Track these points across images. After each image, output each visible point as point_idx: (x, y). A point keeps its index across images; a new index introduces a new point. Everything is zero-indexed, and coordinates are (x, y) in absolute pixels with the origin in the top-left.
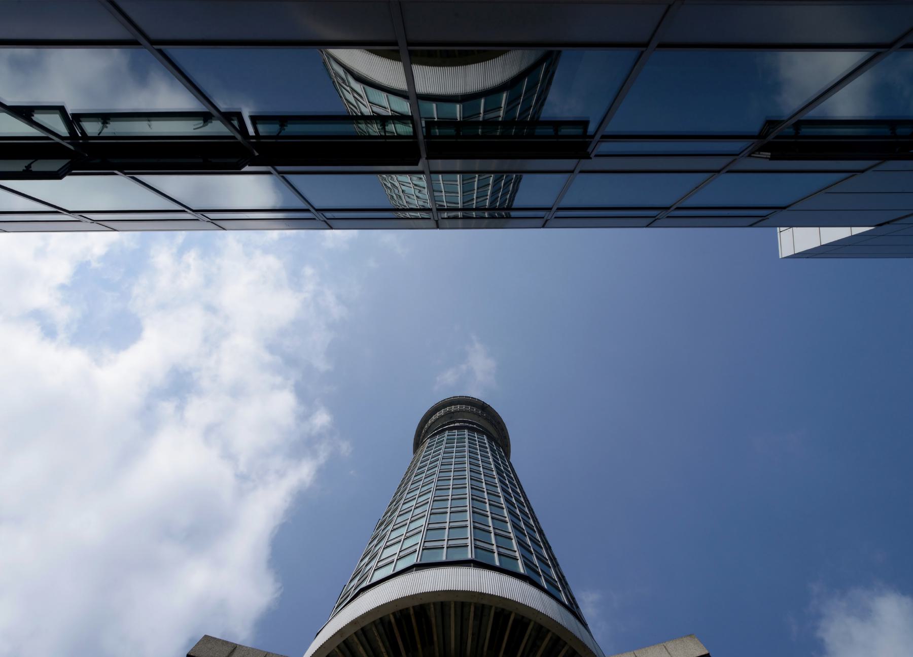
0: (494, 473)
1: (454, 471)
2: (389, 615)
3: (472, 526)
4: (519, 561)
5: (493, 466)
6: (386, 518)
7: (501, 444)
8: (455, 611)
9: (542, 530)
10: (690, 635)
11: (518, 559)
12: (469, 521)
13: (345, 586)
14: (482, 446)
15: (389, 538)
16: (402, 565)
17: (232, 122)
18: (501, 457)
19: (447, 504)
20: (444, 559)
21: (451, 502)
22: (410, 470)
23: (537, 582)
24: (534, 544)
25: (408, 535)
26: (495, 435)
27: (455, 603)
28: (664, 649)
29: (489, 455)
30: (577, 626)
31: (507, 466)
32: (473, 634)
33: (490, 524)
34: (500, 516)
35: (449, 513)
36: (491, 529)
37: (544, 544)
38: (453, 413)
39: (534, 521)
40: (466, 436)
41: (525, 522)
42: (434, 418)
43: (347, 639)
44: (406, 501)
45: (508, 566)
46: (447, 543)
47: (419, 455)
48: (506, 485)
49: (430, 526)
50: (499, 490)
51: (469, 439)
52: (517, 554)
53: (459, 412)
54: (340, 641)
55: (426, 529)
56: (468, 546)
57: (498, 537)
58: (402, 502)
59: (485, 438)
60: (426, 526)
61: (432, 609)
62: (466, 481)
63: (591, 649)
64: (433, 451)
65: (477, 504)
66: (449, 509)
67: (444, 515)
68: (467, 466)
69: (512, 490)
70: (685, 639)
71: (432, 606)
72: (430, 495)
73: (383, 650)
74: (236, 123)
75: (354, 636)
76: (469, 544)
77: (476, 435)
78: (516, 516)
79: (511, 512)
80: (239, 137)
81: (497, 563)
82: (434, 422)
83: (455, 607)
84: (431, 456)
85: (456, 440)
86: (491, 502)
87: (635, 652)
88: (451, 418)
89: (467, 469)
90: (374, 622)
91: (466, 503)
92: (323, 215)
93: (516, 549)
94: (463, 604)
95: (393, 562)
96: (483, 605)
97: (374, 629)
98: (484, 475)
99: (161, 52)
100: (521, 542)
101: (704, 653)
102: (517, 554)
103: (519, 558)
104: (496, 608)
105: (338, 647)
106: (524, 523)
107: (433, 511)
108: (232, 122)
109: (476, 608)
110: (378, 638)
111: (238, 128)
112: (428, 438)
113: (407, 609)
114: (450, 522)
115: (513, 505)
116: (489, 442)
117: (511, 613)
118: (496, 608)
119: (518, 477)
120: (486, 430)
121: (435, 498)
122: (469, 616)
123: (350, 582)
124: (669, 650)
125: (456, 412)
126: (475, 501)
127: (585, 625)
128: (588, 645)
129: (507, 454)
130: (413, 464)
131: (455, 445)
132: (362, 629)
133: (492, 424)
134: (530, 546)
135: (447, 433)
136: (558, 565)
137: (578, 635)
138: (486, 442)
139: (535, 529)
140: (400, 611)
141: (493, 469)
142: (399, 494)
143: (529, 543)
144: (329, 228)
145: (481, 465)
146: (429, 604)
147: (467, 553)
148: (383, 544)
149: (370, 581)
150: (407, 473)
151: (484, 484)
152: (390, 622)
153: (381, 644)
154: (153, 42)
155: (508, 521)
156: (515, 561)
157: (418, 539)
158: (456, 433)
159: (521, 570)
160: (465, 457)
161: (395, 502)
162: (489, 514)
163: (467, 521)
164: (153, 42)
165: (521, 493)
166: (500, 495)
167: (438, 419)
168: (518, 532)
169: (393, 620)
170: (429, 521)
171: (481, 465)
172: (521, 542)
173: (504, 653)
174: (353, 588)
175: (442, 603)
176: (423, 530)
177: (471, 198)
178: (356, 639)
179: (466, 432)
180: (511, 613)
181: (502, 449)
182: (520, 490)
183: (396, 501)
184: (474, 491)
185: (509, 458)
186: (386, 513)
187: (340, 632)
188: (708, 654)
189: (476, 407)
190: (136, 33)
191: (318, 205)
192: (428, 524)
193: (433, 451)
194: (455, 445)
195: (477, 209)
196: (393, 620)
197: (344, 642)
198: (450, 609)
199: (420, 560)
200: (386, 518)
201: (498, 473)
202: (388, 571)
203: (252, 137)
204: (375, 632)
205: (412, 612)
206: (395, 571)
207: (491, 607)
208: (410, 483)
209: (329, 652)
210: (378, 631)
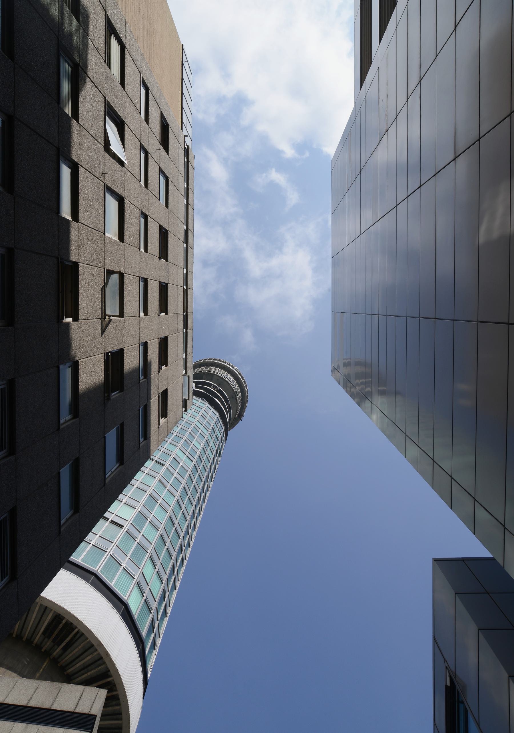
104: (113, 679)
125: (237, 400)
205: (115, 693)
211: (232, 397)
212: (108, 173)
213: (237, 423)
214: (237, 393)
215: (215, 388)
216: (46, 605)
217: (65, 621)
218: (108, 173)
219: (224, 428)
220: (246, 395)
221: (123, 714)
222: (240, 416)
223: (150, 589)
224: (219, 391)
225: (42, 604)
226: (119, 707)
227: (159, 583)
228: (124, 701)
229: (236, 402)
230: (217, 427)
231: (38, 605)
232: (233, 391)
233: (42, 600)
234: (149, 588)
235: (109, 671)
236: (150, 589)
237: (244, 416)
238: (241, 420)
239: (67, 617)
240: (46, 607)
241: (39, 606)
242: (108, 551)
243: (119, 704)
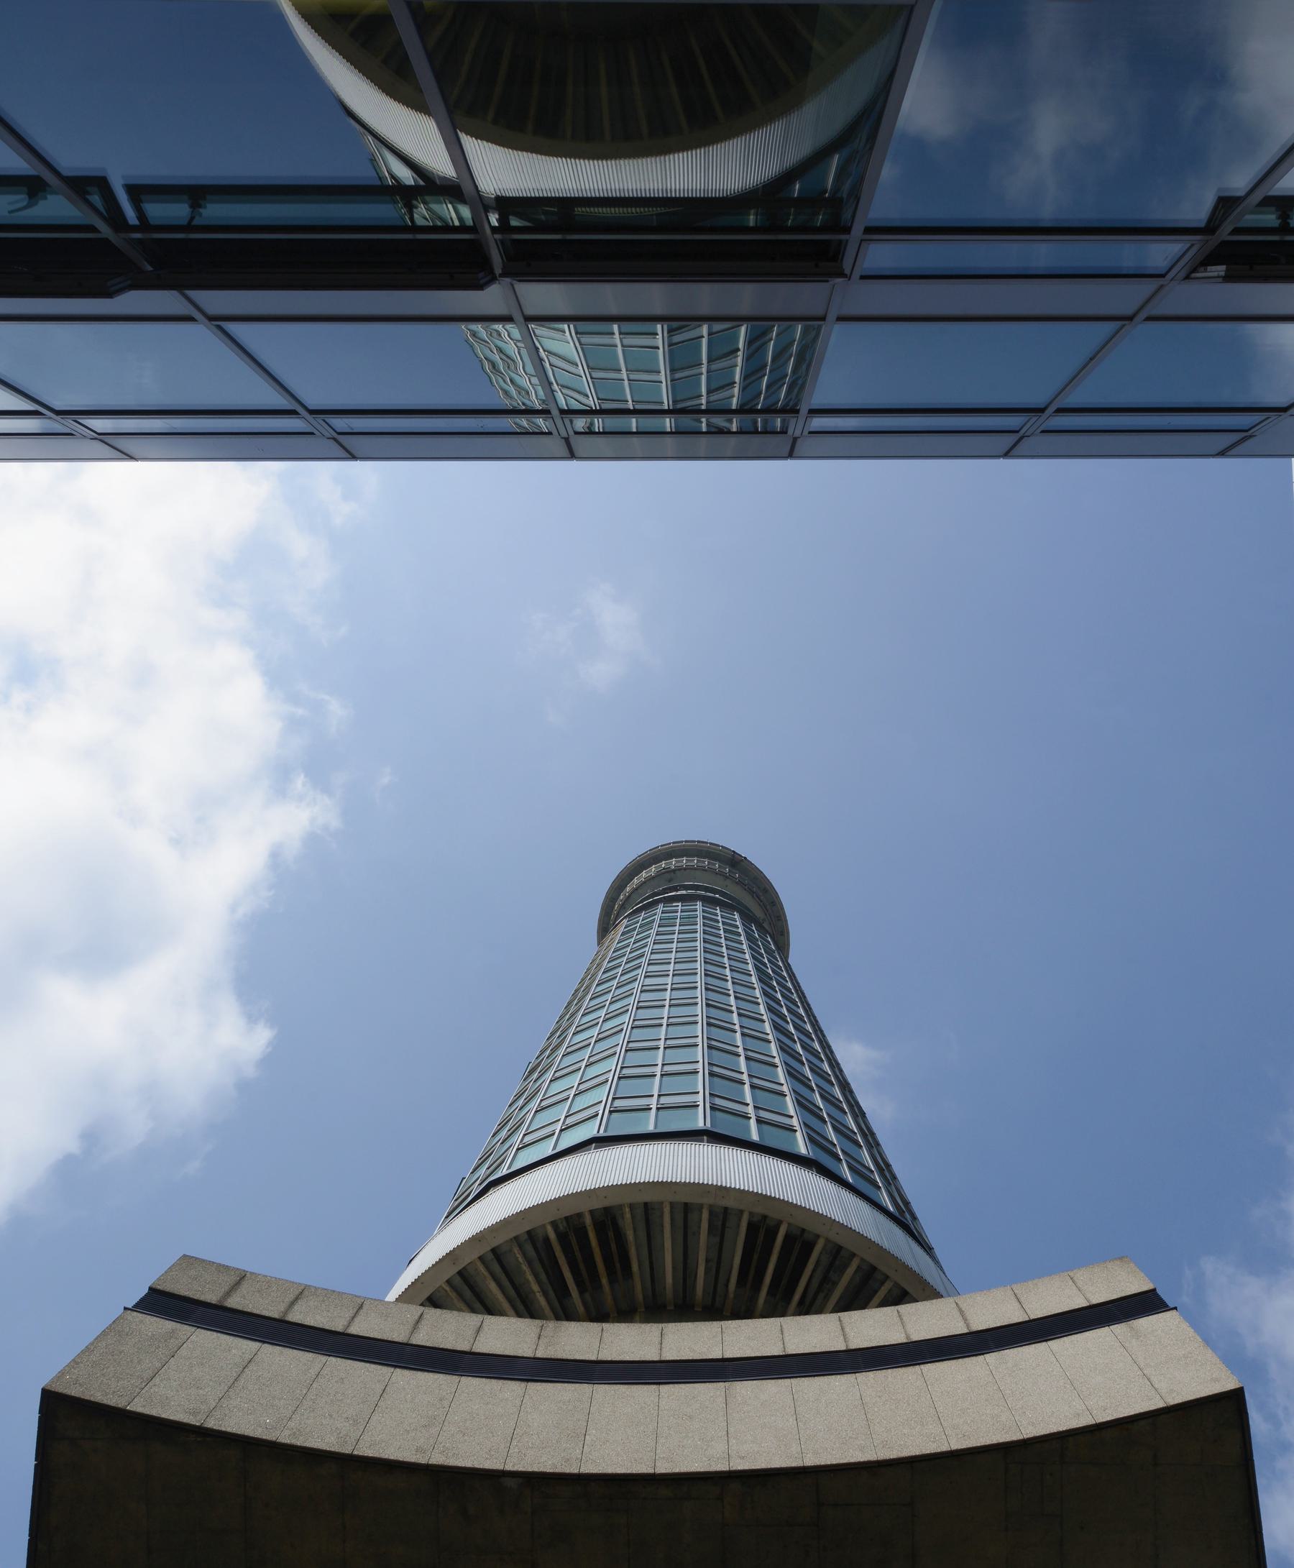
0: (754, 979)
1: (673, 975)
2: (544, 1226)
3: (707, 1072)
4: (799, 1134)
5: (750, 967)
6: (543, 1059)
7: (769, 930)
8: (672, 1219)
9: (848, 1084)
10: (1121, 1258)
11: (786, 1095)
12: (700, 1036)
13: (530, 1063)
14: (731, 932)
15: (579, 1021)
16: (567, 1142)
17: (88, 197)
18: (769, 951)
19: (656, 1057)
20: (651, 1128)
21: (667, 1029)
22: (590, 975)
23: (836, 1173)
24: (829, 1106)
25: (591, 1060)
26: (758, 913)
27: (672, 1204)
28: (1071, 1283)
29: (744, 947)
30: (909, 1246)
31: (789, 990)
32: (707, 1261)
33: (749, 1099)
34: (756, 1013)
35: (662, 1049)
36: (750, 1110)
37: (864, 1135)
38: (674, 871)
39: (831, 1066)
40: (699, 913)
41: (796, 1025)
42: (636, 881)
43: (464, 1268)
44: (578, 1029)
45: (776, 1139)
46: (658, 1101)
47: (598, 965)
48: (783, 1018)
49: (618, 1103)
50: (767, 1027)
51: (704, 918)
52: (795, 1122)
53: (685, 869)
54: (452, 1271)
55: (644, 972)
56: (698, 1072)
57: (757, 1091)
58: (572, 1030)
59: (737, 916)
60: (638, 995)
61: (628, 1216)
62: (696, 1010)
63: (935, 1287)
64: (633, 940)
65: (719, 1057)
66: (662, 1041)
67: (652, 1052)
68: (699, 980)
69: (782, 995)
70: (1109, 1265)
71: (627, 1210)
72: (626, 1018)
73: (535, 1287)
74: (96, 199)
75: (479, 1264)
76: (701, 1104)
77: (718, 911)
78: (804, 1082)
79: (793, 1074)
80: (105, 231)
81: (755, 1137)
82: (636, 889)
83: (672, 1212)
84: (629, 949)
85: (678, 921)
86: (750, 1054)
87: (1014, 1287)
88: (670, 881)
89: (699, 1000)
90: (516, 1238)
91: (696, 1084)
92: (326, 423)
93: (792, 1112)
94: (687, 1207)
95: (553, 1134)
96: (726, 1209)
97: (516, 1250)
98: (733, 983)
99: (220, 328)
100: (815, 1136)
101: (1238, 1386)
102: (795, 1122)
103: (798, 1128)
104: (751, 1214)
105: (448, 1282)
106: (822, 1096)
107: (631, 1045)
108: (88, 197)
109: (711, 1213)
110: (525, 1267)
111: (105, 214)
112: (625, 917)
113: (580, 1215)
114: (663, 1065)
115: (797, 1057)
116: (743, 924)
117: (780, 1223)
118: (751, 1214)
119: (803, 988)
120: (739, 903)
121: (636, 1023)
122: (700, 1227)
123: (472, 1173)
124: (1080, 1284)
125: (679, 869)
126: (712, 1028)
127: (928, 1249)
128: (929, 1280)
129: (782, 946)
130: (596, 964)
131: (677, 928)
132: (494, 1251)
133: (751, 892)
134: (821, 1110)
135: (661, 907)
136: (878, 1144)
137: (911, 1263)
138: (738, 923)
139: (823, 1057)
140: (566, 1218)
141: (752, 973)
142: (567, 1017)
143: (832, 1136)
144: (346, 455)
145: (729, 978)
146: (621, 1207)
147: (696, 1119)
148: (534, 1105)
149: (509, 1168)
150: (583, 980)
151: (732, 998)
152: (547, 1239)
153: (531, 1278)
154: (212, 318)
155: (788, 1093)
156: (781, 1098)
157: (602, 1094)
158: (680, 908)
159: (802, 1148)
160: (697, 950)
161: (559, 1033)
162: (745, 1077)
163: (698, 1062)
164: (212, 318)
165: (815, 1031)
166: (765, 1018)
167: (645, 882)
168: (796, 1083)
169: (552, 1235)
170: (623, 1063)
171: (727, 965)
172: (815, 1136)
173: (768, 1293)
174: (478, 1182)
175: (646, 1204)
176: (601, 1112)
177: (733, 348)
178: (482, 1268)
179: (699, 905)
180: (780, 1223)
181: (771, 938)
182: (813, 1025)
183: (561, 1029)
184: (712, 1010)
185: (787, 958)
186: (542, 1052)
187: (451, 1256)
188: (1154, 1290)
189: (720, 861)
190: (293, 402)
191: (314, 401)
192: (622, 1068)
193: (633, 940)
194: (677, 928)
195: (740, 411)
196: (552, 1235)
197: (460, 1273)
198: (662, 1216)
199: (605, 1131)
200: (543, 1059)
201: (761, 980)
202: (547, 1149)
203: (134, 229)
204: (518, 1256)
205: (588, 1220)
206: (559, 1149)
207: (741, 1212)
208: (589, 996)
209: (431, 1292)
210: (524, 1255)
228: (605, 1197)
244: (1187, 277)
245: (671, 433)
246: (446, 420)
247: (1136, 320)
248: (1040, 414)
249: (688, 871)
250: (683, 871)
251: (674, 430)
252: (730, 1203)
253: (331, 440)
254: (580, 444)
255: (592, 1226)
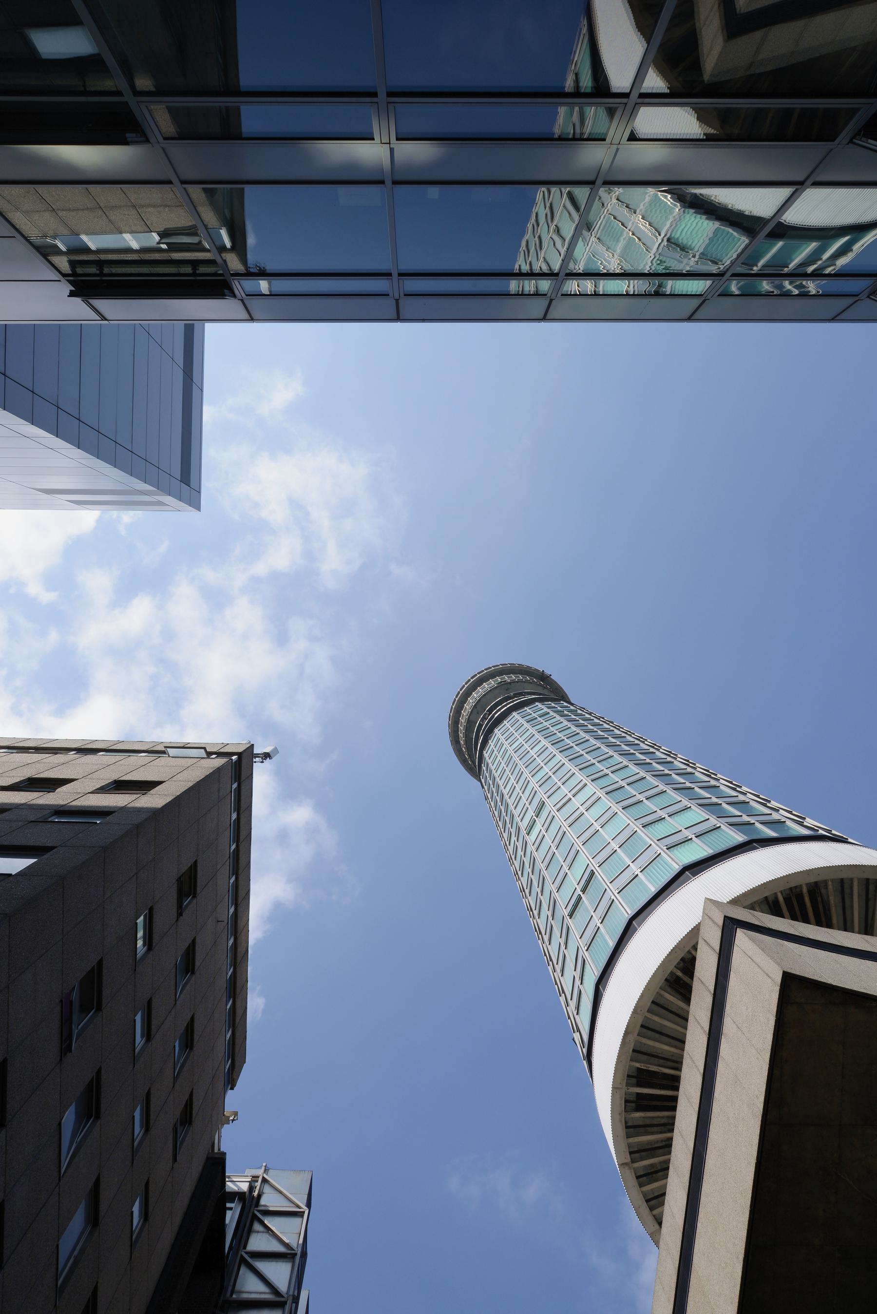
104: (781, 892)
125: (513, 682)
180: (776, 898)
205: (805, 890)
211: (507, 690)
212: (223, 921)
213: (555, 682)
214: (501, 682)
215: (484, 718)
216: (649, 1004)
217: (679, 971)
218: (223, 921)
219: (537, 704)
220: (509, 667)
221: (841, 877)
222: (544, 678)
223: (685, 829)
224: (490, 711)
225: (647, 1010)
226: (830, 883)
227: (689, 813)
228: (819, 875)
229: (516, 683)
230: (531, 714)
231: (651, 1017)
232: (496, 687)
233: (641, 1010)
234: (683, 830)
235: (766, 898)
236: (685, 829)
237: (543, 671)
238: (551, 675)
239: (671, 968)
240: (653, 1002)
241: (651, 1015)
242: (613, 897)
243: (825, 882)
244: (851, 141)
245: (591, 295)
246: (341, 281)
247: (807, 183)
248: (720, 278)
249: (519, 683)
250: (516, 683)
251: (636, 293)
252: (844, 875)
253: (240, 301)
254: (407, 305)
255: (807, 893)
